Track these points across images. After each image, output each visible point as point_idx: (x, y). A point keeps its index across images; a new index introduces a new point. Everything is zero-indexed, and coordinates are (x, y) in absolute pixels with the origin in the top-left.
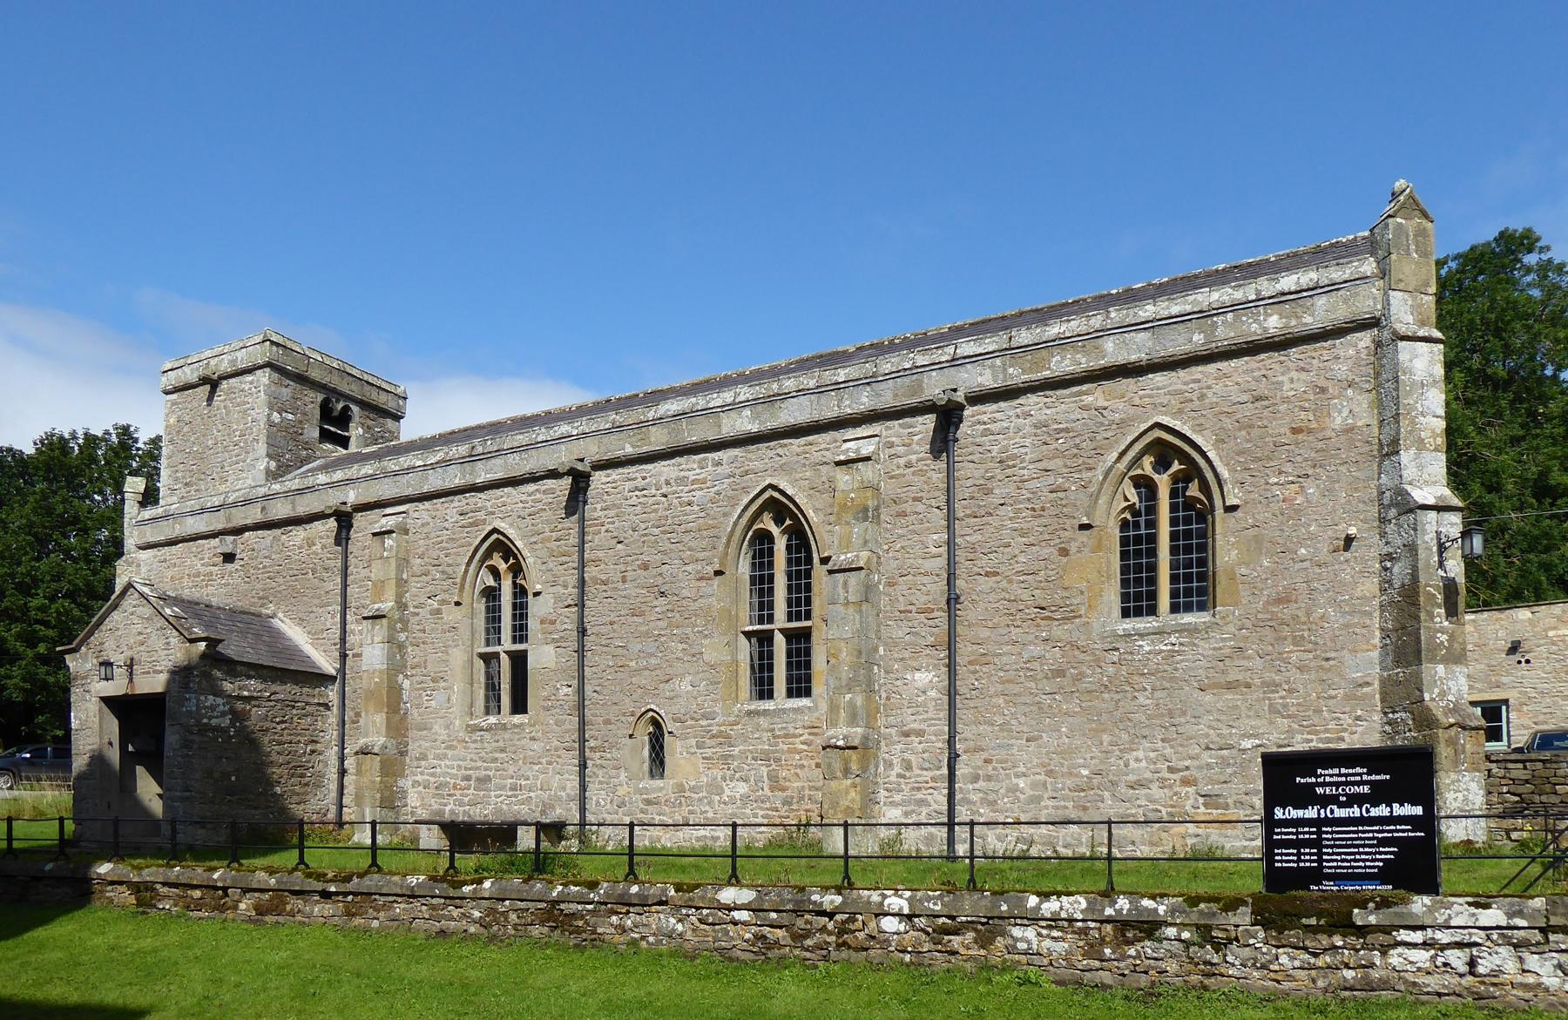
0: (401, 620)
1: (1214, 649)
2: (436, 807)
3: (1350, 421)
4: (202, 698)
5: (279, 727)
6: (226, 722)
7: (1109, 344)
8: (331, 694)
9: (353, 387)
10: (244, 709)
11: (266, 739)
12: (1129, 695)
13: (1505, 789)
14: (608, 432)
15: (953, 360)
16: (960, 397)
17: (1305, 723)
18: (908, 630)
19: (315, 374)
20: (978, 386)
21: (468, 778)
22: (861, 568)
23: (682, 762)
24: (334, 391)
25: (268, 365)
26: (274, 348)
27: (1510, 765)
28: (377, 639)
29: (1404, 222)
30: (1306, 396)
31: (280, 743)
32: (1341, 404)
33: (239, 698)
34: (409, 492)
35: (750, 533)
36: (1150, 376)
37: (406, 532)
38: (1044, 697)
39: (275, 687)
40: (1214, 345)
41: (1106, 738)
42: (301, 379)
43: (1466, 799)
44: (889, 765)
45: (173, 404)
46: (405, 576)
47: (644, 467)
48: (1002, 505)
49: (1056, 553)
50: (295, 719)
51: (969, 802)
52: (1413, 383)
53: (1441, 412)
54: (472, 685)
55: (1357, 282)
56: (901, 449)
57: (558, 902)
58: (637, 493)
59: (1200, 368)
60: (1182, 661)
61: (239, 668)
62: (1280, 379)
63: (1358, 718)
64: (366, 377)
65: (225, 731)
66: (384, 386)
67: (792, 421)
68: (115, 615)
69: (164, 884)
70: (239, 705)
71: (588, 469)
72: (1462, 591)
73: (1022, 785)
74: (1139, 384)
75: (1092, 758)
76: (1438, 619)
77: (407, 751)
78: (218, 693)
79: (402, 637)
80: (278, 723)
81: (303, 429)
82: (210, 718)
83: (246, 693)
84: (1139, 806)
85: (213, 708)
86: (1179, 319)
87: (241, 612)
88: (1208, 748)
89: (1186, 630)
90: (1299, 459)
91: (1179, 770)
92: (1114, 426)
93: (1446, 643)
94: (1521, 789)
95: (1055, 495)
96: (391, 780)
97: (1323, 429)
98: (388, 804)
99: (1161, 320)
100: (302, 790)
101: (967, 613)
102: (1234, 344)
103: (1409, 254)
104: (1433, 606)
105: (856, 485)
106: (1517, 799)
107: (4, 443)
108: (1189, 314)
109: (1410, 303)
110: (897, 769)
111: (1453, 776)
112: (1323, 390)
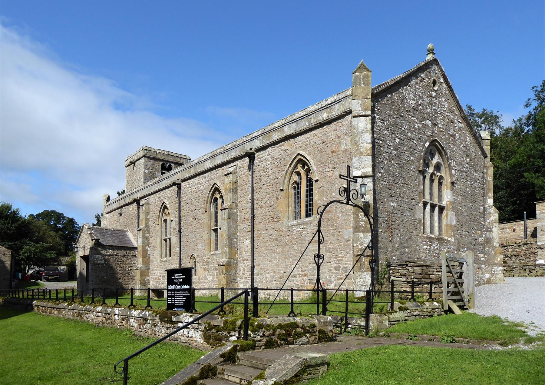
0: (147, 230)
1: (312, 229)
2: (155, 285)
3: (346, 147)
4: (95, 256)
5: (120, 263)
6: (103, 262)
7: (286, 128)
8: (136, 253)
9: (172, 159)
10: (108, 259)
11: (116, 266)
12: (292, 246)
13: (413, 277)
14: (183, 170)
15: (251, 139)
16: (253, 151)
17: (334, 254)
18: (244, 227)
19: (159, 157)
20: (257, 146)
21: (160, 276)
22: (227, 208)
23: (199, 270)
24: (165, 161)
25: (144, 156)
26: (145, 151)
27: (415, 268)
28: (140, 236)
29: (359, 74)
30: (335, 140)
32: (344, 142)
33: (106, 255)
34: (149, 193)
35: (213, 198)
36: (298, 137)
37: (148, 204)
38: (273, 247)
39: (118, 252)
40: (311, 125)
41: (287, 261)
42: (154, 159)
43: (364, 281)
44: (240, 270)
45: (128, 170)
46: (148, 217)
47: (191, 180)
48: (264, 184)
49: (276, 199)
50: (125, 260)
51: (257, 282)
52: (358, 132)
54: (162, 249)
55: (345, 98)
56: (242, 169)
57: (79, 310)
58: (190, 188)
59: (309, 133)
60: (304, 234)
61: (106, 247)
62: (329, 134)
63: (347, 253)
64: (176, 155)
65: (102, 264)
66: (183, 157)
67: (218, 163)
68: (82, 234)
69: (41, 306)
70: (107, 257)
71: (180, 182)
73: (268, 276)
74: (295, 141)
75: (284, 267)
77: (150, 269)
78: (100, 254)
79: (148, 235)
80: (119, 262)
81: (155, 173)
82: (97, 261)
83: (108, 254)
84: (294, 283)
85: (98, 258)
86: (302, 118)
87: (117, 231)
88: (310, 264)
89: (305, 223)
90: (333, 162)
91: (304, 271)
92: (289, 156)
93: (364, 225)
94: (418, 277)
95: (275, 180)
96: (144, 277)
97: (339, 151)
98: (143, 284)
99: (298, 118)
100: (128, 281)
101: (257, 221)
102: (316, 124)
103: (360, 85)
104: (359, 212)
105: (229, 182)
106: (417, 280)
108: (305, 115)
109: (360, 103)
110: (242, 272)
111: (359, 273)
112: (339, 137)
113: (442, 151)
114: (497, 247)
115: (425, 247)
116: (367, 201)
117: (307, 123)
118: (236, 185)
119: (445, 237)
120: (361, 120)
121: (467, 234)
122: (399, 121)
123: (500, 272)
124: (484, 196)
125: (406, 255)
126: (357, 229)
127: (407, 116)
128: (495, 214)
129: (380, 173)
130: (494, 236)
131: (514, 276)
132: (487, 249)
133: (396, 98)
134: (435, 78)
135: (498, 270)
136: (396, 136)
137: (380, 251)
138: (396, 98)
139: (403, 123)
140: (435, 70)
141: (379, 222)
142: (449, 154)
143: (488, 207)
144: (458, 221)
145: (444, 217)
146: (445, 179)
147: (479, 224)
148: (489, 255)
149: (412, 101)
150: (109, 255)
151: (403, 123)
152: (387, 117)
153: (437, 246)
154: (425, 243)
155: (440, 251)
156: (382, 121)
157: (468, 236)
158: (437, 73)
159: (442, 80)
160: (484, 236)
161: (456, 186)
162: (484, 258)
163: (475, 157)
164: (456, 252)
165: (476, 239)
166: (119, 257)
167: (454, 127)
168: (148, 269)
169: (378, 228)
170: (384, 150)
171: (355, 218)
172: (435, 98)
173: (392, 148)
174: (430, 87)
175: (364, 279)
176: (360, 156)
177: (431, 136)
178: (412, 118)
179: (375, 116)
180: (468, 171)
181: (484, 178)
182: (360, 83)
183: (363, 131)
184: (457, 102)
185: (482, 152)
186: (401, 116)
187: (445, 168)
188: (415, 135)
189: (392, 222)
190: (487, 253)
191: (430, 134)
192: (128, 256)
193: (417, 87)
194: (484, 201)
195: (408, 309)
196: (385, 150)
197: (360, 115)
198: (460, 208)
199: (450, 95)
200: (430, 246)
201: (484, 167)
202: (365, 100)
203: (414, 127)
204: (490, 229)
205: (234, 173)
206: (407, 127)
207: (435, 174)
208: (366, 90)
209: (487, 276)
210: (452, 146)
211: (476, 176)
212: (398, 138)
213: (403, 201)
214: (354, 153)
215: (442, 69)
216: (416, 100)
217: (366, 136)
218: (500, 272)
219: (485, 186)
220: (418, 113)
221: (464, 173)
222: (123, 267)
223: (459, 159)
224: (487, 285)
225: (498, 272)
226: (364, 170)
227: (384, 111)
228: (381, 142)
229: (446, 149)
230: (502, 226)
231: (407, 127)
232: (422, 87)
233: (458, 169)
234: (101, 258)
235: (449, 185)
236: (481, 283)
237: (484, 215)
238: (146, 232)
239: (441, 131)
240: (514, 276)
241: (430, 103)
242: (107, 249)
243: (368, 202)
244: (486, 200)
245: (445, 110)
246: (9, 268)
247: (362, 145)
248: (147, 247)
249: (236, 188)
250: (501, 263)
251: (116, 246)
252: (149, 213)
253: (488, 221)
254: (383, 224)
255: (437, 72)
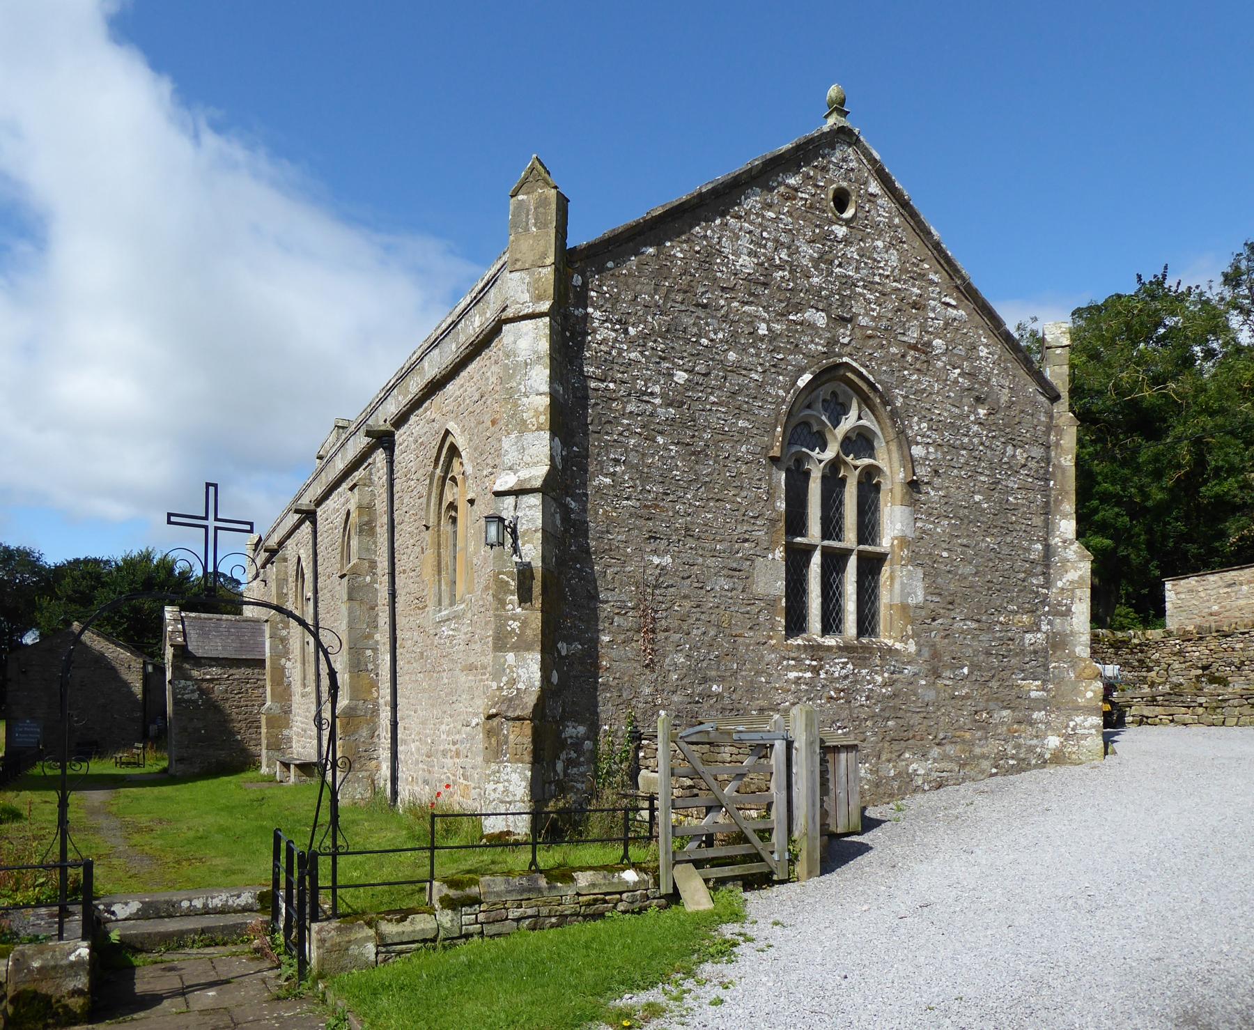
5: (237, 697)
10: (208, 688)
11: (227, 705)
29: (525, 197)
31: (238, 707)
39: (231, 671)
43: (506, 790)
50: (250, 690)
53: (545, 388)
61: (203, 661)
65: (195, 702)
70: (205, 685)
72: (538, 575)
76: (510, 607)
77: (291, 710)
79: (284, 633)
80: (236, 694)
82: (183, 694)
83: (208, 677)
85: (185, 688)
102: (467, 348)
103: (527, 229)
104: (505, 593)
107: (13, 542)
109: (526, 281)
113: (871, 395)
114: (1084, 660)
115: (792, 675)
116: (528, 560)
117: (454, 347)
118: (369, 515)
119: (886, 641)
120: (524, 330)
121: (974, 625)
122: (688, 320)
123: (1093, 731)
124: (1046, 514)
125: (712, 702)
126: (501, 642)
127: (722, 302)
128: (1082, 565)
129: (606, 475)
130: (1076, 628)
131: (1224, 722)
132: (1053, 665)
133: (680, 255)
134: (845, 184)
135: (1087, 724)
136: (674, 363)
137: (603, 696)
138: (680, 255)
139: (707, 324)
140: (844, 160)
141: (602, 615)
142: (901, 400)
143: (1060, 544)
144: (933, 589)
145: (885, 582)
146: (888, 473)
147: (1022, 594)
148: (1060, 681)
149: (744, 259)
150: (211, 680)
151: (707, 324)
152: (640, 313)
153: (842, 668)
154: (792, 662)
155: (855, 682)
156: (618, 327)
157: (978, 632)
158: (852, 170)
159: (874, 187)
160: (1044, 628)
161: (928, 493)
162: (1043, 690)
163: (1013, 403)
164: (923, 682)
165: (1012, 640)
166: (236, 683)
167: (926, 320)
168: (286, 713)
169: (599, 631)
170: (624, 408)
171: (497, 609)
172: (847, 241)
173: (658, 401)
174: (824, 211)
175: (506, 784)
176: (521, 432)
177: (825, 353)
178: (746, 308)
179: (587, 314)
180: (982, 444)
181: (1048, 460)
182: (527, 224)
183: (528, 361)
184: (937, 246)
185: (1040, 384)
186: (697, 305)
187: (887, 443)
188: (758, 355)
189: (656, 612)
190: (1054, 675)
191: (820, 348)
192: (258, 680)
193: (771, 215)
194: (1048, 527)
195: (480, 903)
196: (629, 408)
197: (519, 317)
198: (945, 554)
199: (910, 229)
200: (816, 670)
201: (1049, 428)
202: (540, 269)
203: (750, 333)
204: (1064, 608)
205: (365, 485)
206: (720, 335)
207: (846, 463)
208: (542, 243)
209: (1053, 741)
210: (915, 377)
211: (1014, 456)
212: (685, 371)
213: (703, 549)
214: (507, 426)
215: (871, 154)
216: (764, 254)
217: (535, 373)
218: (1093, 731)
219: (1052, 483)
220: (771, 293)
221: (964, 452)
222: (247, 706)
223: (943, 413)
224: (1050, 769)
225: (1086, 732)
226: (524, 474)
227: (627, 295)
228: (612, 386)
229: (888, 389)
230: (1229, 577)
231: (720, 335)
232: (791, 216)
233: (939, 441)
234: (191, 687)
235: (899, 491)
236: (1029, 764)
237: (1047, 566)
238: (280, 626)
239: (870, 337)
240: (1224, 722)
241: (824, 260)
242: (204, 665)
243: (530, 563)
244: (1053, 523)
245: (886, 273)
246: (140, 696)
247: (525, 400)
248: (284, 660)
249: (369, 523)
250: (1094, 704)
251: (227, 658)
252: (287, 581)
253: (1060, 584)
254: (616, 619)
255: (853, 165)
